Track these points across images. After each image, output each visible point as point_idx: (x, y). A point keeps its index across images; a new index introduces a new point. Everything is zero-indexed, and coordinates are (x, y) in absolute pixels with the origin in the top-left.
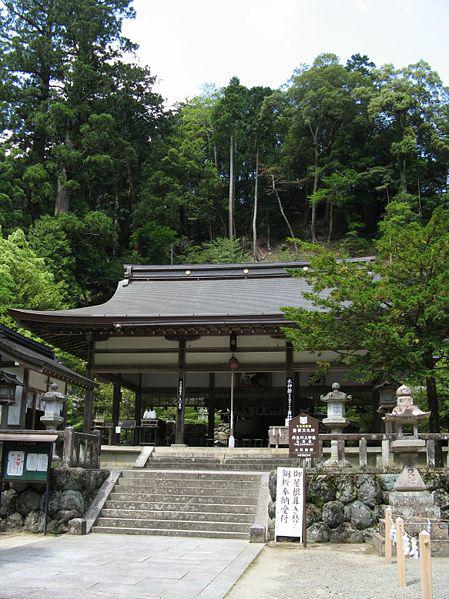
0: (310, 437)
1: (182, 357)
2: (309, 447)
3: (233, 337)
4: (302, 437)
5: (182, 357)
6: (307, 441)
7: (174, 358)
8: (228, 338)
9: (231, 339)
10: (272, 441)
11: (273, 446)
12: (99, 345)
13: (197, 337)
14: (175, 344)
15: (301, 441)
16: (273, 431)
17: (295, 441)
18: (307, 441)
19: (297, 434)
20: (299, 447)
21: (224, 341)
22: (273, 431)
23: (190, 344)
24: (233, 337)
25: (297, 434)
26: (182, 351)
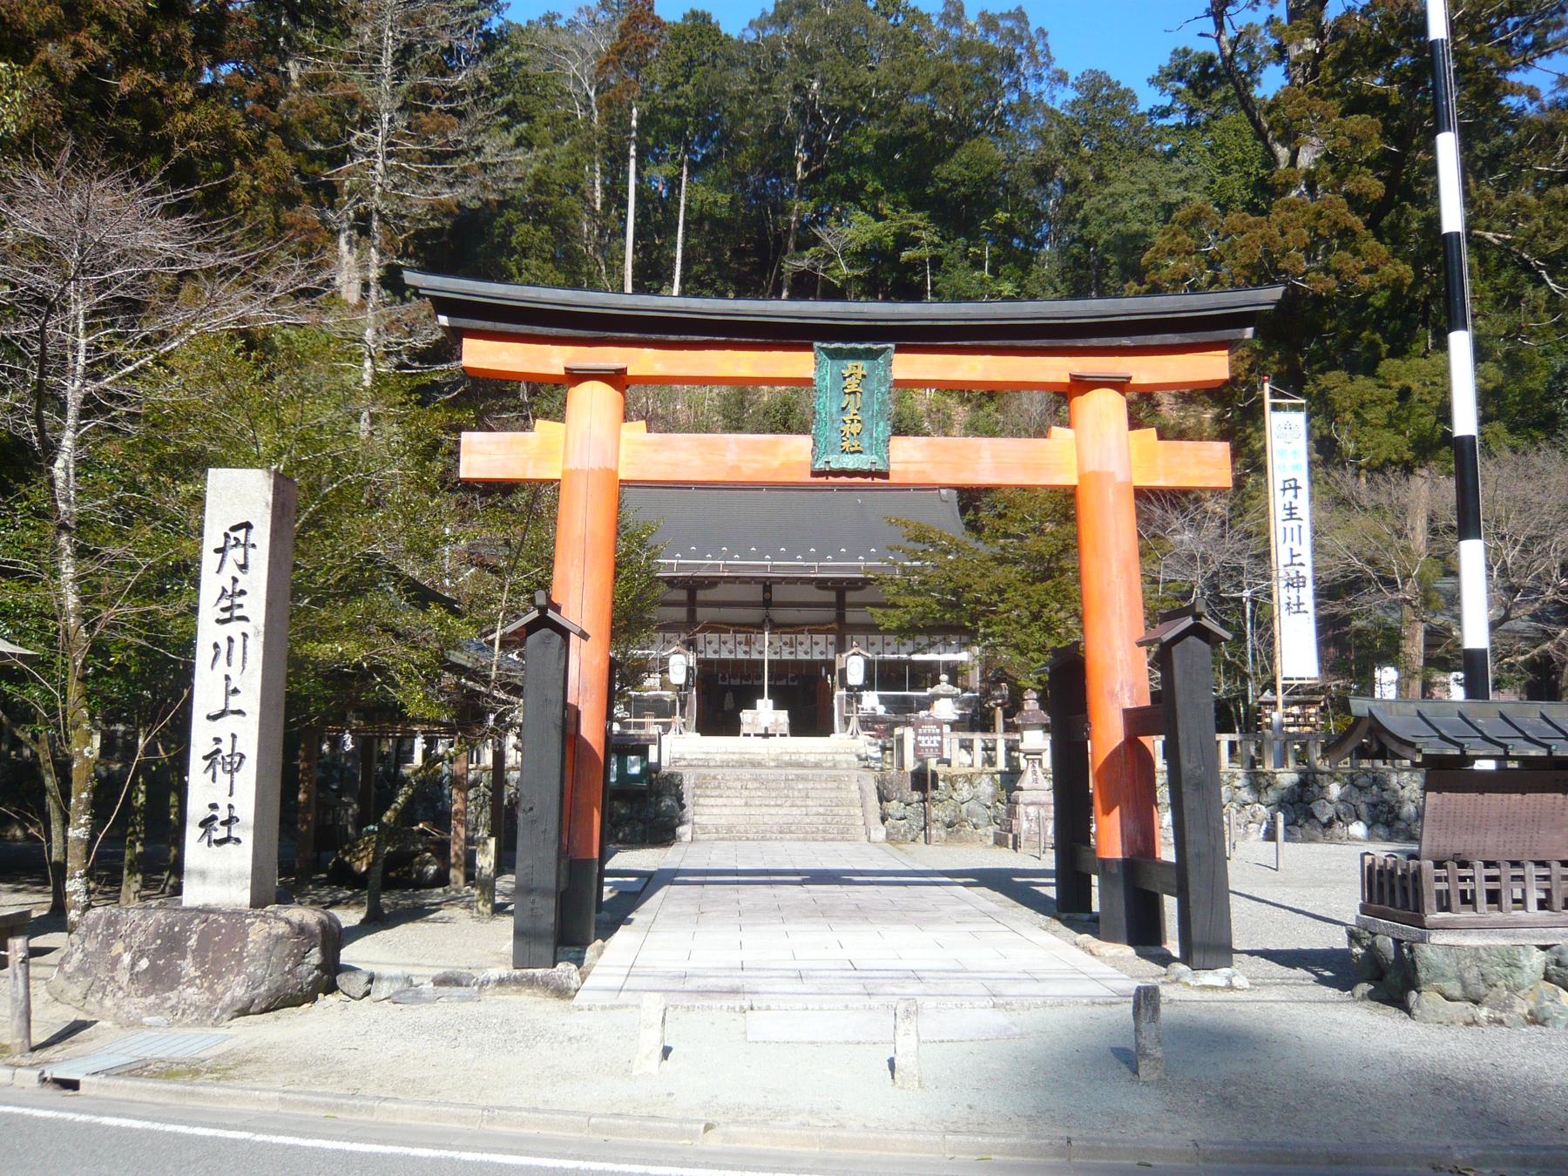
1: (692, 614)
5: (692, 614)
10: (744, 729)
16: (746, 715)
23: (701, 595)
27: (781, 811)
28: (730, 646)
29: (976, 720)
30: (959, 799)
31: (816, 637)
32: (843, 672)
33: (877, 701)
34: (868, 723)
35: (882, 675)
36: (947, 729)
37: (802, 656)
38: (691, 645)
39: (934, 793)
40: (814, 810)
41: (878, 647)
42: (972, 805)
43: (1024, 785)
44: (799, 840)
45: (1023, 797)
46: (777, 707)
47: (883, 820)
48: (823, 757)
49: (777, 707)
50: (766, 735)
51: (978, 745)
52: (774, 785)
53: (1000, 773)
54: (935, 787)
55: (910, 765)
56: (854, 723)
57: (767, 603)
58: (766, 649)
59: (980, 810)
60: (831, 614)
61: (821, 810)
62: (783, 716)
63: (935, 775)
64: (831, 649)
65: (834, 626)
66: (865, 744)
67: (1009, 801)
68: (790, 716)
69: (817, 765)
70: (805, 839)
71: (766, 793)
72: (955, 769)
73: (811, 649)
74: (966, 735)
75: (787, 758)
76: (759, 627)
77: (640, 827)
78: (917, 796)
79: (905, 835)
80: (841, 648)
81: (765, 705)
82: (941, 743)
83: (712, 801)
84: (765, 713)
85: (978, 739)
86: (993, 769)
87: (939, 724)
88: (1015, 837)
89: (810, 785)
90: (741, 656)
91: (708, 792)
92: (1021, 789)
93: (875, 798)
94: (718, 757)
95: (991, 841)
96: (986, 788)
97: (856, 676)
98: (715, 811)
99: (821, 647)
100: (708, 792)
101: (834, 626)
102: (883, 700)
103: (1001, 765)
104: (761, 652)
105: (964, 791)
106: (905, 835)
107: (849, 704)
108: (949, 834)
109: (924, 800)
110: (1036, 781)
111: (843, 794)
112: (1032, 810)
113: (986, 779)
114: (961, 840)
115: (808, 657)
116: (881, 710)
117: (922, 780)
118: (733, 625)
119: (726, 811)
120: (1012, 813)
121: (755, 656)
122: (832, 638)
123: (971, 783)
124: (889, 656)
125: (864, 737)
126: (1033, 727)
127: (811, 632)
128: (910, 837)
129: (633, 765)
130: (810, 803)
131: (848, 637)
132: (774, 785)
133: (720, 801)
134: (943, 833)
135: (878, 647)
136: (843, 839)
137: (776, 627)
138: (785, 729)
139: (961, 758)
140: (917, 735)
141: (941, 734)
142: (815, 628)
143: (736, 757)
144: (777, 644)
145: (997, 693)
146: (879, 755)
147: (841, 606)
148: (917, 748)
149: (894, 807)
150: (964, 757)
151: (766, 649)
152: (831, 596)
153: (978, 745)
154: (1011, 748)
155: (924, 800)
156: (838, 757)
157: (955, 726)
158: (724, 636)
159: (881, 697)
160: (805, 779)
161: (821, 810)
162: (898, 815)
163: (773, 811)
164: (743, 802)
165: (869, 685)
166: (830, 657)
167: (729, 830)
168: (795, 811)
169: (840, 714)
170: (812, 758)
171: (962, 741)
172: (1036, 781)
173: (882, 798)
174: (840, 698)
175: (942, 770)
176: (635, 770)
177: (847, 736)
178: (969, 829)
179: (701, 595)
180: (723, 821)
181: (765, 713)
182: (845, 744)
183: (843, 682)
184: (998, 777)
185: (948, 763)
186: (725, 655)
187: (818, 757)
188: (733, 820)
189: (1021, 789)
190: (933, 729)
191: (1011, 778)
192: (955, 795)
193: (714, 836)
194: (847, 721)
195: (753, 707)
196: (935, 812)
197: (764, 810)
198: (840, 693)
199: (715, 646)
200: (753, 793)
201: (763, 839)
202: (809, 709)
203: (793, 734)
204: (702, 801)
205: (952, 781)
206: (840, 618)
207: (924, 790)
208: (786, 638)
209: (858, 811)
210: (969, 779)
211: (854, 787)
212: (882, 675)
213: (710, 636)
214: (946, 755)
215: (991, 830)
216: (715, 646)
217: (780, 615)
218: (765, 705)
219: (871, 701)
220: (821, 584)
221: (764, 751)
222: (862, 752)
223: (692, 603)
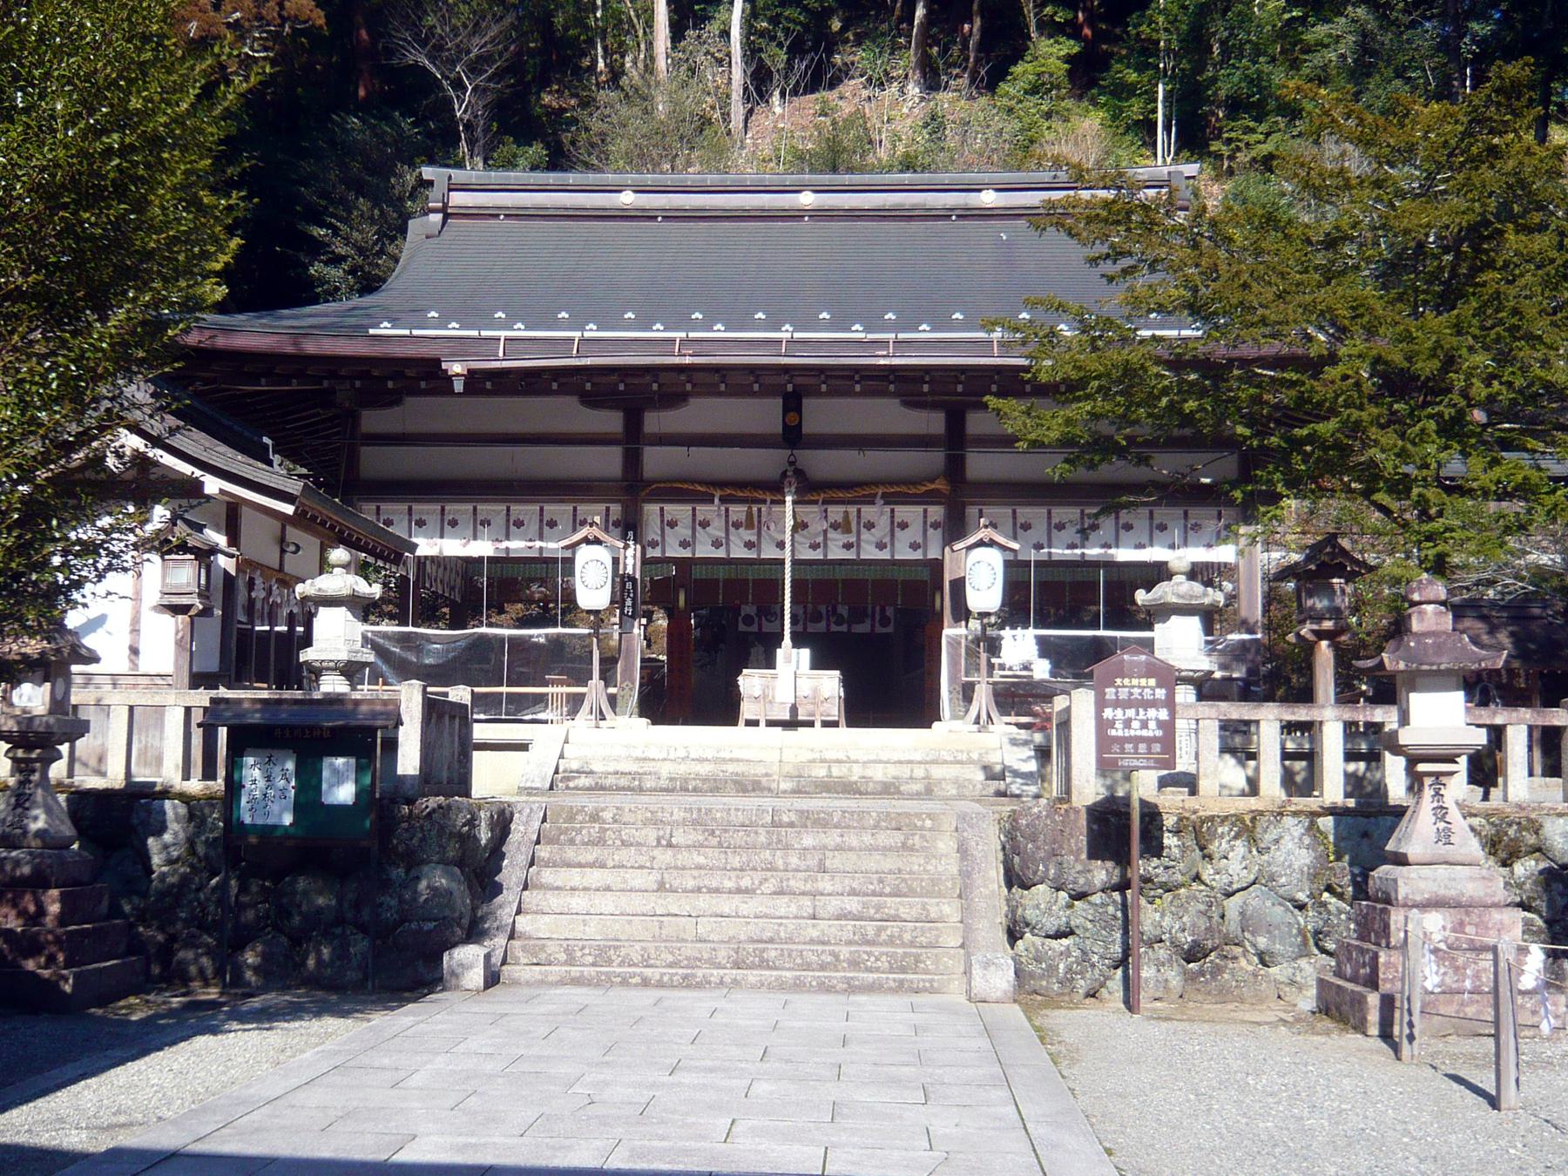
0: (1152, 713)
1: (632, 460)
2: (1150, 741)
3: (793, 403)
4: (1131, 713)
5: (632, 460)
6: (1144, 725)
7: (608, 462)
8: (777, 403)
9: (786, 410)
10: (747, 710)
11: (752, 723)
12: (374, 420)
13: (393, 399)
14: (610, 421)
15: (1127, 723)
16: (750, 681)
17: (1111, 724)
18: (1144, 725)
19: (1153, 704)
20: (1122, 741)
21: (765, 414)
22: (750, 681)
23: (654, 422)
24: (793, 403)
25: (1117, 704)
26: (633, 439)
27: (750, 906)
28: (717, 530)
29: (1269, 672)
30: (1220, 881)
31: (904, 512)
32: (959, 586)
33: (1033, 649)
34: (1017, 698)
35: (1040, 595)
36: (1185, 694)
37: (870, 553)
38: (630, 527)
39: (1144, 866)
40: (834, 904)
41: (1039, 532)
42: (1255, 899)
43: (1413, 850)
44: (781, 986)
45: (1409, 883)
46: (818, 663)
47: (1013, 936)
48: (904, 772)
49: (818, 663)
50: (792, 724)
51: (1269, 739)
52: (739, 837)
53: (1333, 811)
54: (1153, 847)
55: (1088, 788)
56: (983, 697)
57: (792, 437)
58: (789, 537)
59: (1278, 913)
60: (934, 459)
61: (853, 904)
62: (830, 683)
63: (1152, 815)
64: (935, 536)
65: (940, 485)
66: (1004, 743)
67: (1361, 889)
68: (847, 683)
69: (889, 789)
70: (798, 986)
71: (710, 857)
72: (1209, 801)
73: (889, 538)
74: (1237, 711)
75: (820, 772)
76: (774, 489)
77: (360, 946)
78: (1102, 873)
79: (1068, 981)
80: (955, 529)
81: (793, 659)
82: (1168, 727)
83: (574, 877)
84: (792, 677)
85: (1269, 720)
86: (1312, 803)
87: (1169, 677)
88: (1388, 1003)
89: (833, 838)
90: (739, 552)
91: (570, 853)
92: (1401, 860)
93: (996, 874)
94: (666, 770)
95: (1307, 1001)
96: (1293, 852)
97: (985, 593)
98: (578, 902)
99: (913, 533)
100: (570, 853)
101: (940, 485)
102: (1046, 648)
103: (1333, 790)
104: (781, 545)
105: (1234, 861)
106: (1068, 981)
107: (972, 654)
108: (1191, 978)
109: (1123, 886)
110: (1445, 837)
111: (915, 863)
112: (1435, 924)
113: (1293, 828)
114: (1224, 995)
115: (885, 555)
116: (1042, 670)
117: (1118, 831)
118: (722, 484)
119: (606, 903)
120: (1374, 928)
121: (769, 552)
122: (936, 512)
123: (1253, 840)
124: (1060, 552)
125: (1004, 728)
126: (1436, 680)
127: (890, 499)
128: (1082, 985)
129: (339, 778)
130: (825, 884)
131: (972, 511)
132: (739, 837)
133: (595, 877)
134: (1173, 976)
135: (1039, 532)
136: (900, 988)
137: (811, 489)
138: (834, 711)
139: (1212, 769)
140: (1101, 704)
141: (1170, 703)
142: (899, 491)
143: (704, 769)
144: (817, 526)
145: (1320, 604)
146: (1032, 766)
147: (948, 429)
148: (1104, 742)
149: (1041, 902)
150: (1233, 774)
151: (789, 537)
152: (933, 422)
153: (1269, 739)
154: (1369, 745)
155: (1123, 886)
156: (938, 772)
157: (1207, 689)
158: (703, 510)
159: (1041, 641)
160: (821, 822)
161: (853, 904)
162: (1051, 924)
163: (726, 905)
164: (648, 879)
165: (1015, 610)
166: (933, 554)
167: (602, 956)
168: (783, 906)
169: (953, 678)
170: (879, 774)
171: (1228, 727)
172: (1445, 837)
173: (1015, 879)
174: (954, 643)
175: (1172, 802)
176: (344, 793)
177: (965, 726)
178: (1247, 964)
179: (654, 422)
180: (592, 930)
181: (792, 677)
182: (963, 742)
183: (962, 613)
184: (1327, 823)
185: (1190, 783)
186: (704, 550)
187: (893, 771)
188: (617, 927)
189: (1401, 860)
190: (1147, 687)
191: (1367, 828)
192: (1207, 873)
193: (556, 971)
194: (967, 692)
195: (770, 663)
196: (1151, 917)
197: (703, 902)
198: (952, 632)
199: (683, 531)
200: (684, 858)
201: (687, 983)
202: (888, 668)
203: (851, 723)
204: (548, 876)
205: (1199, 832)
206: (955, 468)
207: (1122, 858)
208: (836, 513)
209: (949, 909)
210: (1247, 829)
211: (946, 845)
212: (1040, 595)
213: (672, 510)
214: (1183, 764)
215: (1311, 968)
216: (683, 531)
217: (823, 463)
218: (793, 659)
219: (1021, 649)
220: (906, 384)
221: (773, 757)
222: (994, 759)
223: (633, 439)
